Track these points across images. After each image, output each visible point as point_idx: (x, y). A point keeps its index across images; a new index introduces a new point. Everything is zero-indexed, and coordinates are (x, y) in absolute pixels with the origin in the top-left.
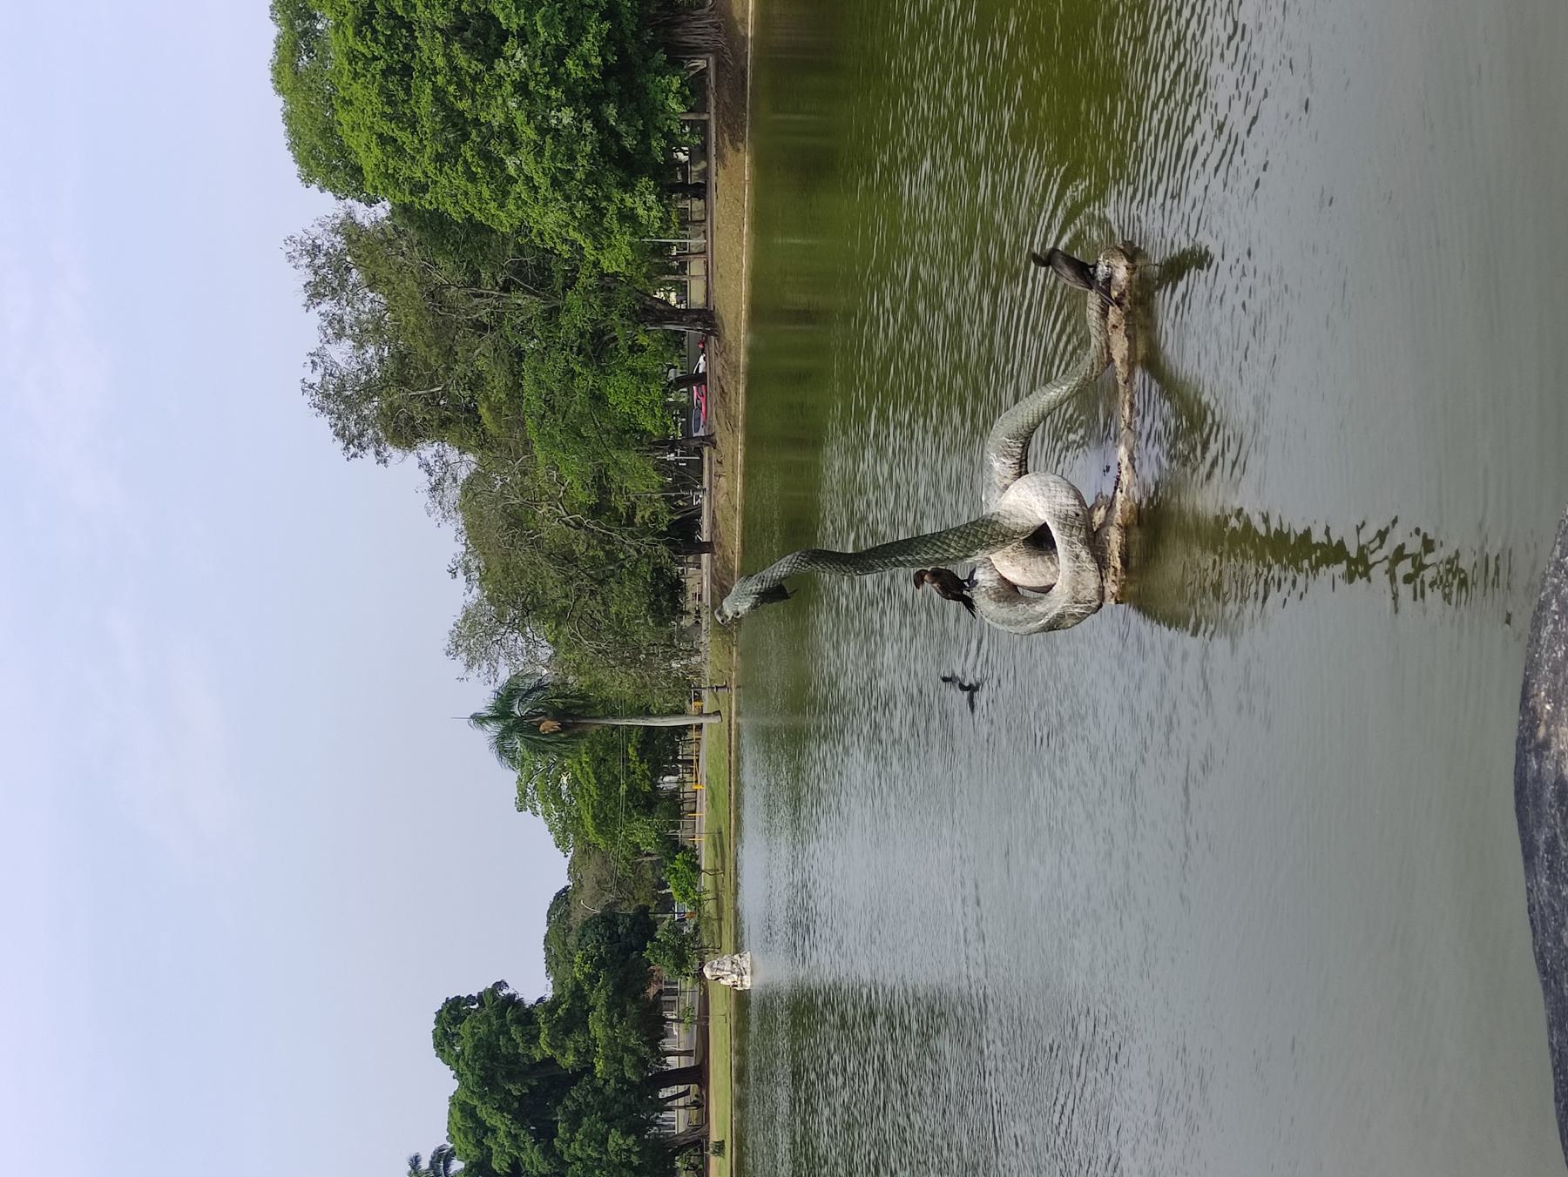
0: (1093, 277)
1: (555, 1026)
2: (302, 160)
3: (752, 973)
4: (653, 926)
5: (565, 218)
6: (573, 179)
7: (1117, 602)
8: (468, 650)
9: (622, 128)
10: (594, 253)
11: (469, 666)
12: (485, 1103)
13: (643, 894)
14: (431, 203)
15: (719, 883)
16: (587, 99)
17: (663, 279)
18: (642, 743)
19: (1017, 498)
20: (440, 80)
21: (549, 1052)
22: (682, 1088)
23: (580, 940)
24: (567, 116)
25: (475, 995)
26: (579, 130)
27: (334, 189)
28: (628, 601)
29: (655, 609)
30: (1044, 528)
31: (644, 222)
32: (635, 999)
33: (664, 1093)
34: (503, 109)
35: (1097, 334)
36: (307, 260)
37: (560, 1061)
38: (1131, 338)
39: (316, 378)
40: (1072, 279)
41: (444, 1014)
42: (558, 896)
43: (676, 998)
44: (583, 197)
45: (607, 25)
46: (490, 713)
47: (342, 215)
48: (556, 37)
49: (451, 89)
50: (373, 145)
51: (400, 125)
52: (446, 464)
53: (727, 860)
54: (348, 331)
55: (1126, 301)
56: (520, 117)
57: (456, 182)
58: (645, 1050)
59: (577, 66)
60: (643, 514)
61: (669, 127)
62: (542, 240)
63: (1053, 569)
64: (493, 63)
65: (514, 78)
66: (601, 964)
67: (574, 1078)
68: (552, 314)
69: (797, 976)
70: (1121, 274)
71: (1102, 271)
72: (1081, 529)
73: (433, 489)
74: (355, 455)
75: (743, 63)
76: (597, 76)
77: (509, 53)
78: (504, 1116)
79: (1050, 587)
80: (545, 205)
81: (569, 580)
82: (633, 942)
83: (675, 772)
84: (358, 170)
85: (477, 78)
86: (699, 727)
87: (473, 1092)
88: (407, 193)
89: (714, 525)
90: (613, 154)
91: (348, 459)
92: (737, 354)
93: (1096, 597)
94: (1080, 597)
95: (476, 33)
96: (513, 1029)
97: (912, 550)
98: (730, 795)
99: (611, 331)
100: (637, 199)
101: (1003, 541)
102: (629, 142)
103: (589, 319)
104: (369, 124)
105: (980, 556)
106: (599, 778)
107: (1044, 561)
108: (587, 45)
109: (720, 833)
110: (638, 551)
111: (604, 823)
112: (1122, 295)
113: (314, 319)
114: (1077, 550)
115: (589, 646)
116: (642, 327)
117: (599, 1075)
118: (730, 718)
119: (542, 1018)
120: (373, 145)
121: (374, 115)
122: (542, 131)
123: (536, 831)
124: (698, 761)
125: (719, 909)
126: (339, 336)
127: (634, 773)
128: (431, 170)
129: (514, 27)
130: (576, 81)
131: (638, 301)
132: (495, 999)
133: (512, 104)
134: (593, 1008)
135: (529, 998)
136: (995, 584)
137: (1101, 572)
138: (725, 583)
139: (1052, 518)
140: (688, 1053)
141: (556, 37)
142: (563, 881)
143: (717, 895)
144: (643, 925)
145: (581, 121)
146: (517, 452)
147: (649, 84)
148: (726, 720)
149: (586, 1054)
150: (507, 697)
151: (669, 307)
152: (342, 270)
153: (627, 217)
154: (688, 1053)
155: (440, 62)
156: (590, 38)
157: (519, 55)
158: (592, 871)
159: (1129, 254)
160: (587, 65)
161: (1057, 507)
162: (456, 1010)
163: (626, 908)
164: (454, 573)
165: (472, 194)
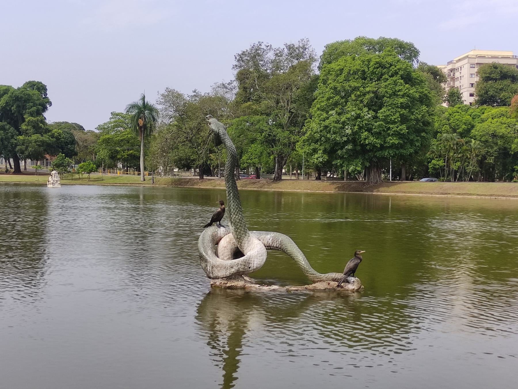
0: (349, 276)
1: (36, 122)
2: (332, 45)
3: (53, 187)
4: (70, 157)
5: (314, 131)
6: (327, 133)
7: (212, 285)
8: (168, 96)
9: (344, 151)
10: (303, 140)
11: (163, 95)
12: (9, 98)
13: (82, 155)
14: (320, 86)
15: (85, 180)
16: (354, 139)
17: (290, 166)
18: (134, 156)
19: (256, 243)
20: (362, 89)
21: (27, 120)
22: (13, 167)
23: (66, 132)
24: (349, 131)
25: (47, 96)
26: (344, 136)
27: (324, 55)
28: (184, 151)
29: (180, 159)
30: (242, 255)
31: (313, 157)
32: (45, 150)
33: (11, 160)
34: (352, 110)
35: (325, 277)
36: (301, 45)
37: (24, 124)
38: (325, 290)
39: (263, 46)
40: (349, 267)
41: (41, 85)
42: (81, 127)
43: (45, 165)
44: (321, 136)
45: (379, 146)
46: (146, 102)
47: (316, 57)
48: (375, 128)
49: (358, 93)
50: (340, 67)
51: (346, 76)
52: (232, 90)
53: (93, 182)
54: (277, 58)
55: (339, 289)
56: (349, 116)
57: (327, 94)
58: (27, 153)
59: (365, 136)
60: (212, 156)
61: (344, 166)
62: (307, 122)
63: (225, 258)
64: (367, 107)
65: (361, 114)
66: (58, 139)
67: (17, 128)
68: (280, 126)
69: (52, 198)
70: (350, 287)
71: (352, 279)
72: (244, 269)
73: (223, 85)
74: (236, 58)
75: (365, 191)
76: (362, 142)
77: (370, 112)
78: (4, 103)
79: (218, 257)
80: (319, 124)
81: (191, 129)
82: (65, 150)
83: (124, 167)
84: (330, 63)
85: (362, 101)
86: (139, 174)
87: (13, 93)
88: (323, 78)
89: (209, 180)
90: (335, 147)
91: (235, 56)
92: (268, 188)
93: (214, 275)
94: (215, 269)
95: (376, 102)
96: (35, 108)
97: (235, 199)
98: (116, 183)
99: (275, 146)
100: (320, 155)
101: (237, 238)
102: (339, 152)
103: (280, 139)
104: (347, 65)
105: (231, 228)
106: (122, 140)
107: (229, 255)
108: (372, 139)
109: (102, 180)
110: (201, 154)
111: (107, 141)
112: (342, 287)
113: (283, 47)
114: (235, 267)
115: (169, 136)
116: (277, 156)
117: (18, 137)
118: (143, 184)
119: (39, 118)
120: (340, 67)
121: (350, 67)
122: (344, 123)
123: (105, 118)
124: (127, 174)
125: (76, 179)
126: (276, 54)
127: (124, 152)
128: (331, 85)
129: (378, 115)
130: (360, 135)
131: (285, 155)
132: (46, 103)
133: (353, 113)
134: (42, 136)
135: (46, 114)
136: (219, 235)
137: (225, 277)
138: (189, 183)
139: (248, 257)
140: (25, 169)
141: (375, 128)
142: (87, 128)
143: (81, 179)
144: (71, 154)
145: (346, 136)
146: (235, 114)
147: (358, 160)
148: (142, 183)
149: (25, 133)
150: (151, 109)
151: (283, 165)
152: (298, 57)
153: (315, 151)
154: (25, 169)
155: (368, 89)
156: (375, 140)
157: (369, 116)
158: (91, 138)
159: (359, 290)
160: (365, 139)
161: (253, 260)
162: (42, 89)
163: (77, 149)
164: (195, 92)
165: (323, 99)
